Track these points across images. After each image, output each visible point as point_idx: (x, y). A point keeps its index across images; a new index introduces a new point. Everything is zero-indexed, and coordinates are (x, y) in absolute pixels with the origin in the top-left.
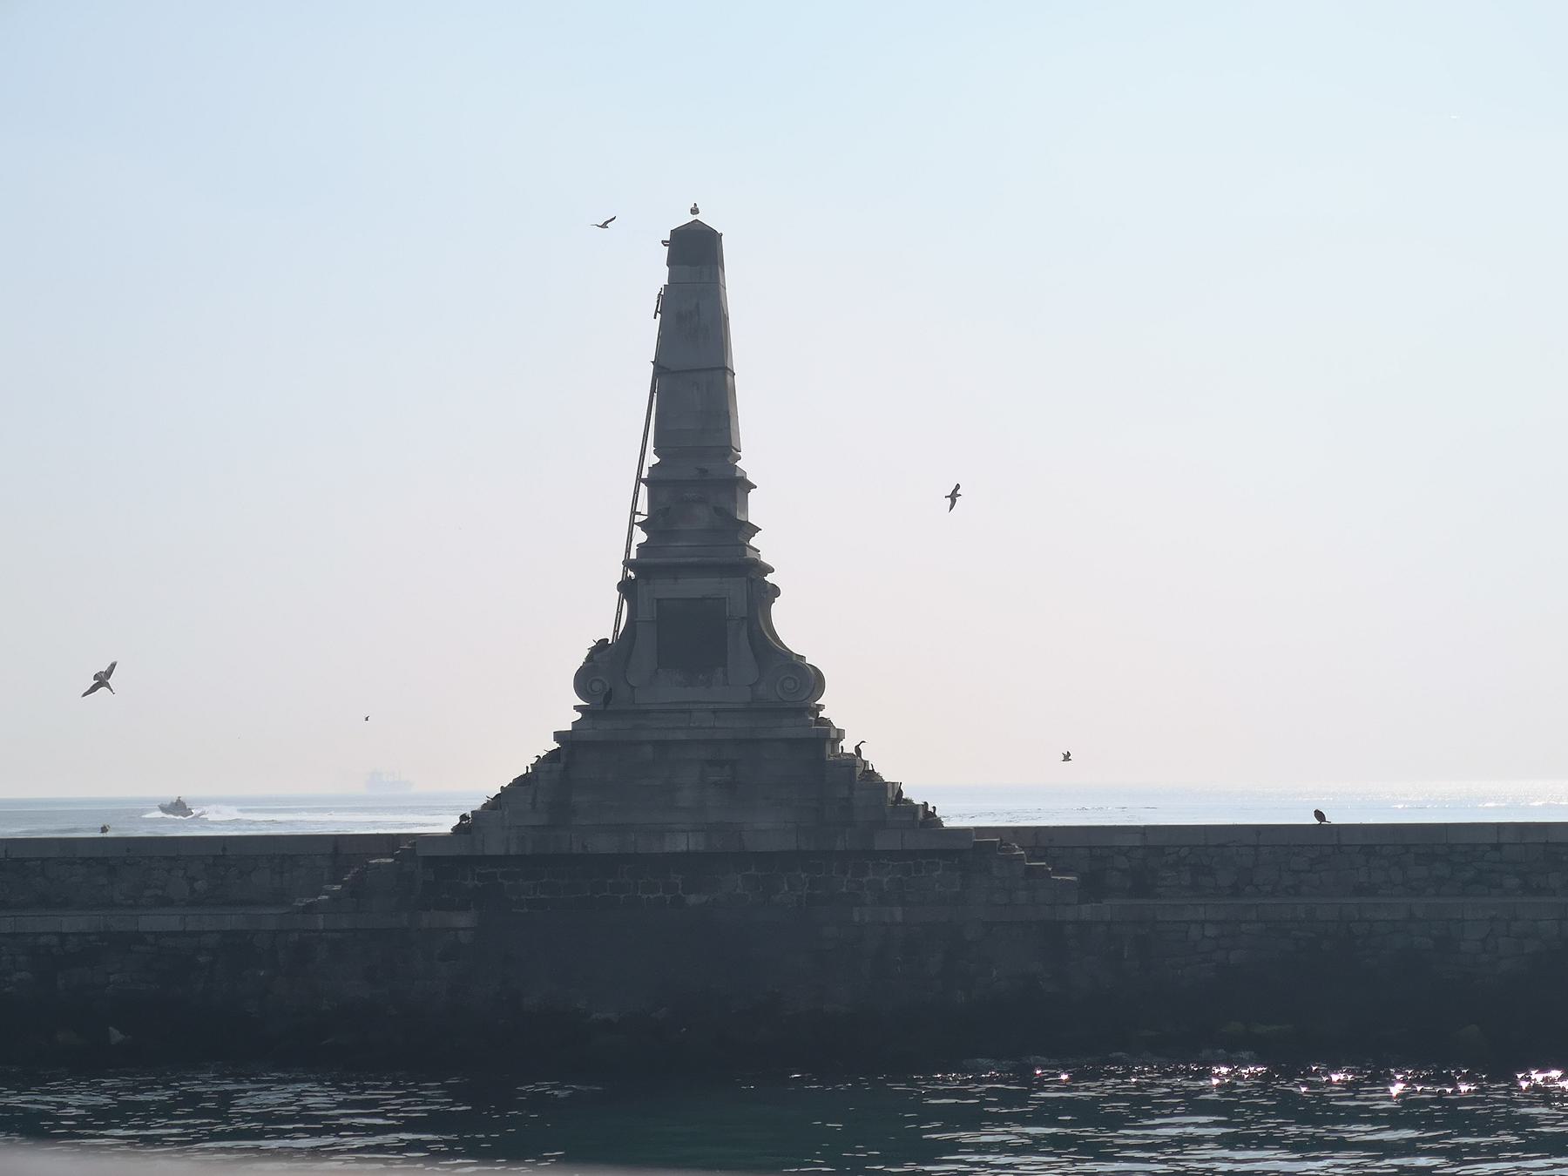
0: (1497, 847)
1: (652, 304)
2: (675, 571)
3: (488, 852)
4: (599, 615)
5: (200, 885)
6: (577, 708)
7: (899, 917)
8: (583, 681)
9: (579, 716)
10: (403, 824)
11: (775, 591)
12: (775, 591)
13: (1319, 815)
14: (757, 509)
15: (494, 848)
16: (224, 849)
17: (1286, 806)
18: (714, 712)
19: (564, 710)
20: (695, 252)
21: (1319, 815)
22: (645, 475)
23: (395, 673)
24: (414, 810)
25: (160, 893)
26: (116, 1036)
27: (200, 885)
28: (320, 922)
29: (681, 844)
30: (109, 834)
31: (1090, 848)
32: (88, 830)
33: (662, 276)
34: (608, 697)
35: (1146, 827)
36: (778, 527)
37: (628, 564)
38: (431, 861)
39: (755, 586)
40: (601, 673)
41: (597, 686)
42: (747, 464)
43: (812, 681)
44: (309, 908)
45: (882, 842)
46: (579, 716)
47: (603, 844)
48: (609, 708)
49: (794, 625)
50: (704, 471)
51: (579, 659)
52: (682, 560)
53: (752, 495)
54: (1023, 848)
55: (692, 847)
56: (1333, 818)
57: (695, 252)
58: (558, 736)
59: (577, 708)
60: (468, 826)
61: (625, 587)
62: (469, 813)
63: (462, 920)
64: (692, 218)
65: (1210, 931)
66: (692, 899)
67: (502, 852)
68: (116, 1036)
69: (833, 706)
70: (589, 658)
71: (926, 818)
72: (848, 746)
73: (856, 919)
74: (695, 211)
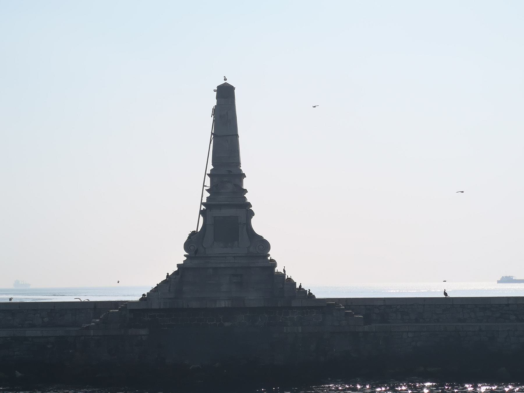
0: (508, 305)
1: (210, 112)
2: (220, 206)
3: (153, 307)
4: (194, 222)
6: (185, 255)
7: (300, 330)
8: (187, 246)
9: (186, 258)
10: (51, 299)
13: (445, 294)
14: (246, 184)
15: (155, 306)
16: (54, 307)
17: (434, 290)
18: (234, 257)
19: (180, 256)
20: (226, 94)
21: (445, 294)
22: (209, 172)
23: (114, 243)
24: (23, 294)
25: (31, 322)
26: (18, 374)
28: (92, 333)
29: (223, 304)
30: (12, 301)
31: (366, 306)
32: (18, 301)
33: (214, 102)
34: (196, 252)
35: (385, 298)
36: (256, 189)
37: (202, 204)
38: (132, 311)
39: (247, 211)
40: (193, 243)
41: (192, 248)
42: (244, 168)
43: (265, 245)
44: (88, 328)
45: (294, 304)
46: (186, 258)
47: (194, 305)
48: (197, 255)
49: (259, 225)
50: (230, 171)
51: (508, 276)
52: (223, 203)
53: (245, 180)
54: (343, 305)
55: (227, 306)
56: (450, 295)
57: (226, 94)
58: (178, 265)
59: (185, 255)
60: (144, 299)
61: (202, 212)
62: (146, 294)
63: (144, 332)
65: (410, 335)
66: (227, 324)
67: (158, 308)
68: (18, 374)
70: (189, 238)
71: (311, 296)
72: (279, 269)
73: (285, 331)
74: (225, 80)
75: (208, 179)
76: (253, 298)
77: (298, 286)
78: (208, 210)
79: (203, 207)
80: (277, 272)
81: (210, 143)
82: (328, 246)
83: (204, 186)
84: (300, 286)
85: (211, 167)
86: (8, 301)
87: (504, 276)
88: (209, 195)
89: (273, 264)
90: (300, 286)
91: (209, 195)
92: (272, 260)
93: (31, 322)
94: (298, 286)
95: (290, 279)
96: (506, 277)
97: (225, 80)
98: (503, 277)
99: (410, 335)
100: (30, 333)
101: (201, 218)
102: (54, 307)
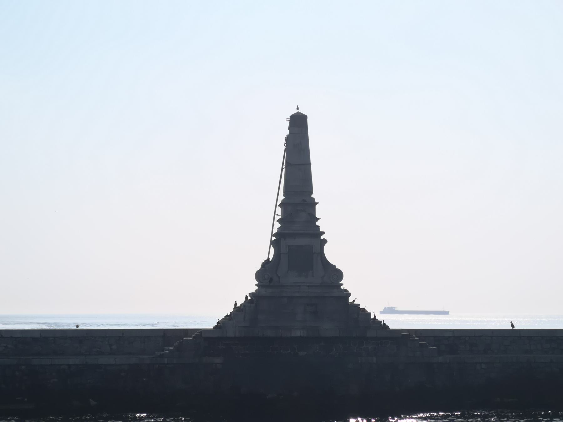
4: (264, 252)
5: (114, 347)
8: (259, 275)
9: (257, 288)
11: (325, 241)
12: (325, 241)
13: (513, 326)
14: (319, 212)
15: (230, 334)
16: (123, 334)
18: (308, 286)
20: (298, 123)
21: (513, 326)
22: (279, 202)
25: (98, 350)
26: (93, 403)
27: (114, 347)
28: (166, 361)
29: (297, 333)
30: (80, 328)
34: (271, 280)
36: (326, 218)
37: (272, 236)
43: (339, 274)
46: (257, 288)
49: (331, 254)
50: (304, 200)
51: (390, 307)
54: (417, 337)
55: (302, 335)
56: (517, 327)
57: (298, 123)
60: (221, 325)
61: (272, 243)
63: (218, 360)
64: (296, 111)
66: (301, 353)
68: (93, 403)
69: (346, 284)
74: (298, 109)
75: (279, 210)
76: (328, 328)
77: (372, 317)
78: (278, 241)
79: (274, 238)
80: (241, 305)
81: (282, 169)
82: (407, 275)
83: (275, 214)
84: (375, 316)
85: (281, 197)
86: (75, 328)
87: (387, 306)
88: (279, 225)
89: (347, 294)
90: (375, 316)
91: (279, 225)
92: (346, 290)
93: (98, 350)
94: (372, 317)
95: (363, 310)
96: (389, 308)
97: (298, 109)
98: (385, 308)
99: (484, 366)
100: (103, 360)
101: (272, 249)
102: (123, 334)
